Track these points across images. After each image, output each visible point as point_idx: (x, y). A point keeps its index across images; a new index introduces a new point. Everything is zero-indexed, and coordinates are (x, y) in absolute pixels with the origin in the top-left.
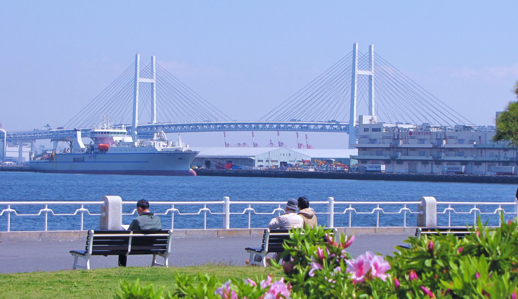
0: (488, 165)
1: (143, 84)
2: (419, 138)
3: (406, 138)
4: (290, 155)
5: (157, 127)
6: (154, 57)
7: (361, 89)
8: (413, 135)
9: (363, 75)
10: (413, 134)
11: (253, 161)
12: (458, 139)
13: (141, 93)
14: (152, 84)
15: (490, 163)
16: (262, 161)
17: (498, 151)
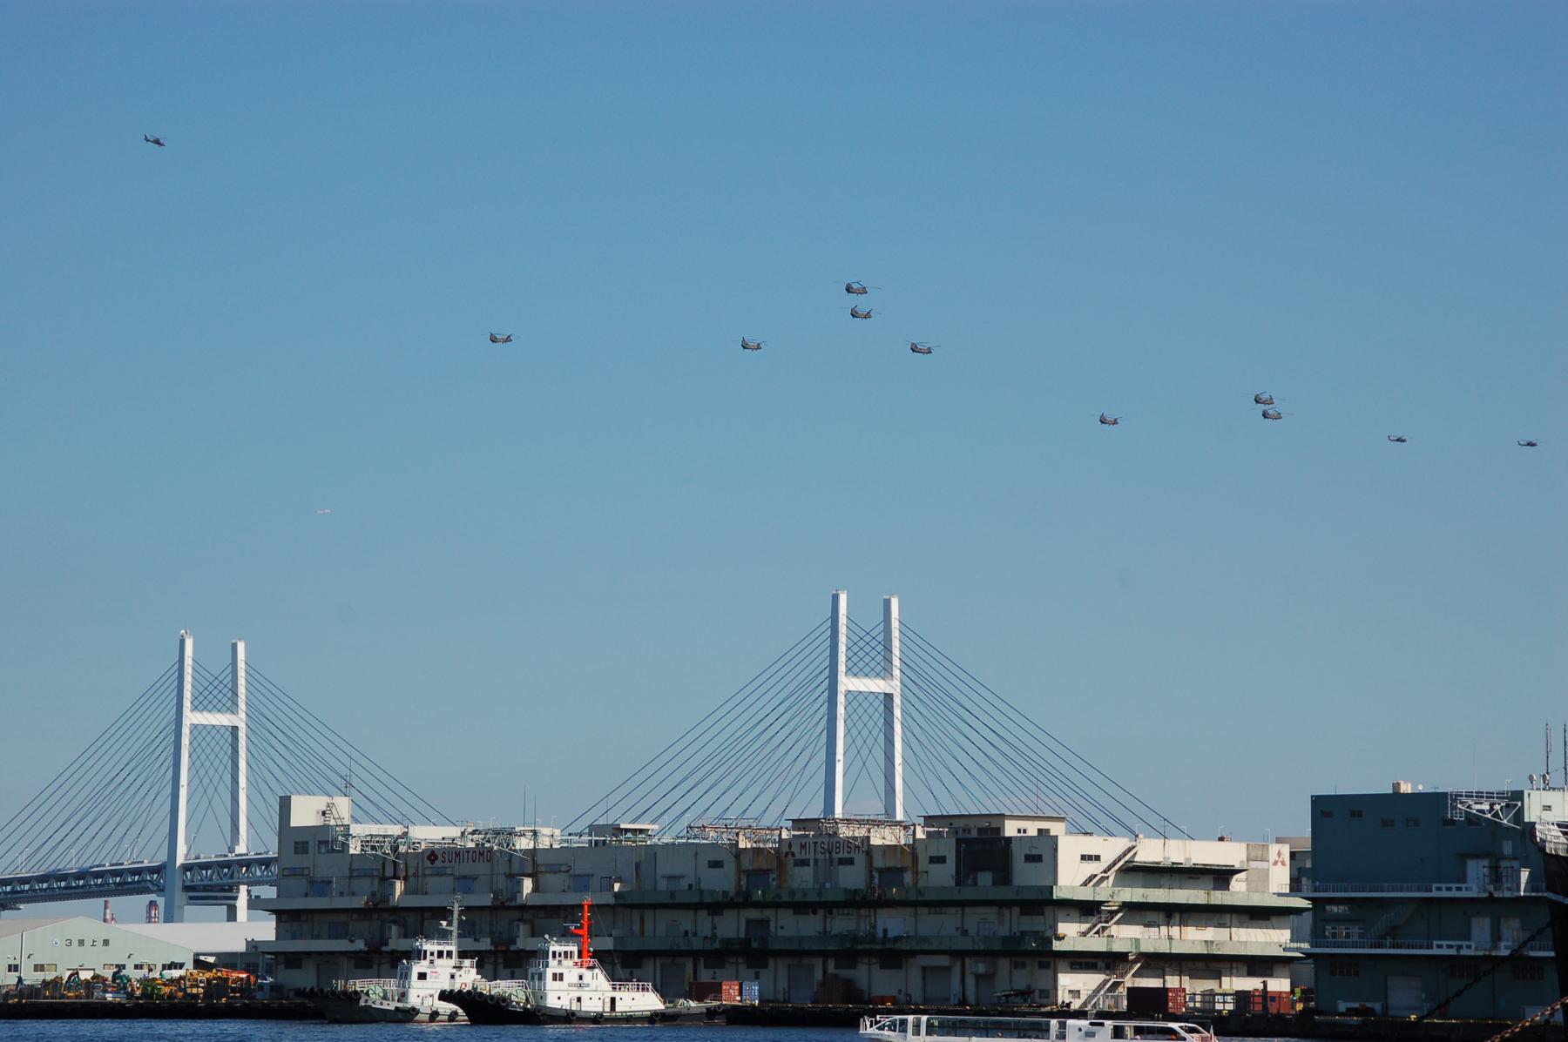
0: (662, 965)
1: (214, 731)
2: (457, 873)
3: (420, 874)
4: (106, 942)
5: (248, 864)
6: (241, 647)
7: (859, 742)
8: (438, 863)
10: (440, 857)
12: (572, 872)
14: (235, 728)
15: (669, 960)
17: (690, 915)
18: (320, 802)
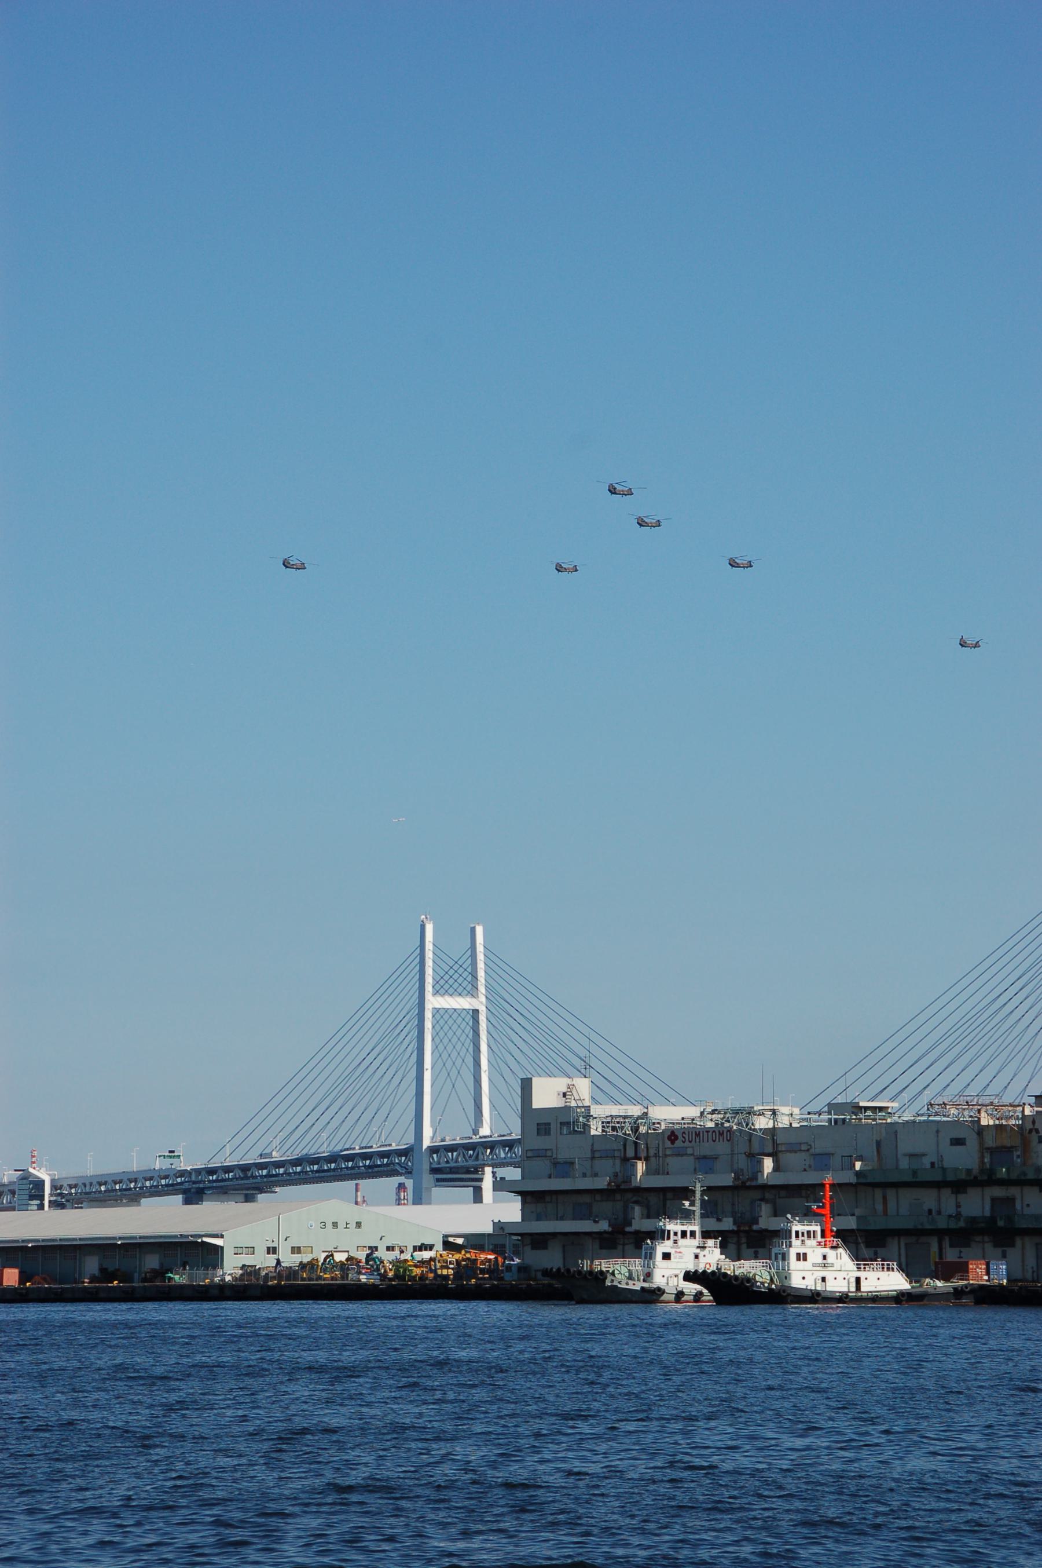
0: (906, 1244)
4: (359, 1225)
5: (492, 1145)
8: (678, 1143)
9: (446, 1010)
11: (218, 1250)
12: (812, 1151)
13: (441, 1047)
14: (476, 1012)
16: (252, 1250)
18: (561, 1084)
